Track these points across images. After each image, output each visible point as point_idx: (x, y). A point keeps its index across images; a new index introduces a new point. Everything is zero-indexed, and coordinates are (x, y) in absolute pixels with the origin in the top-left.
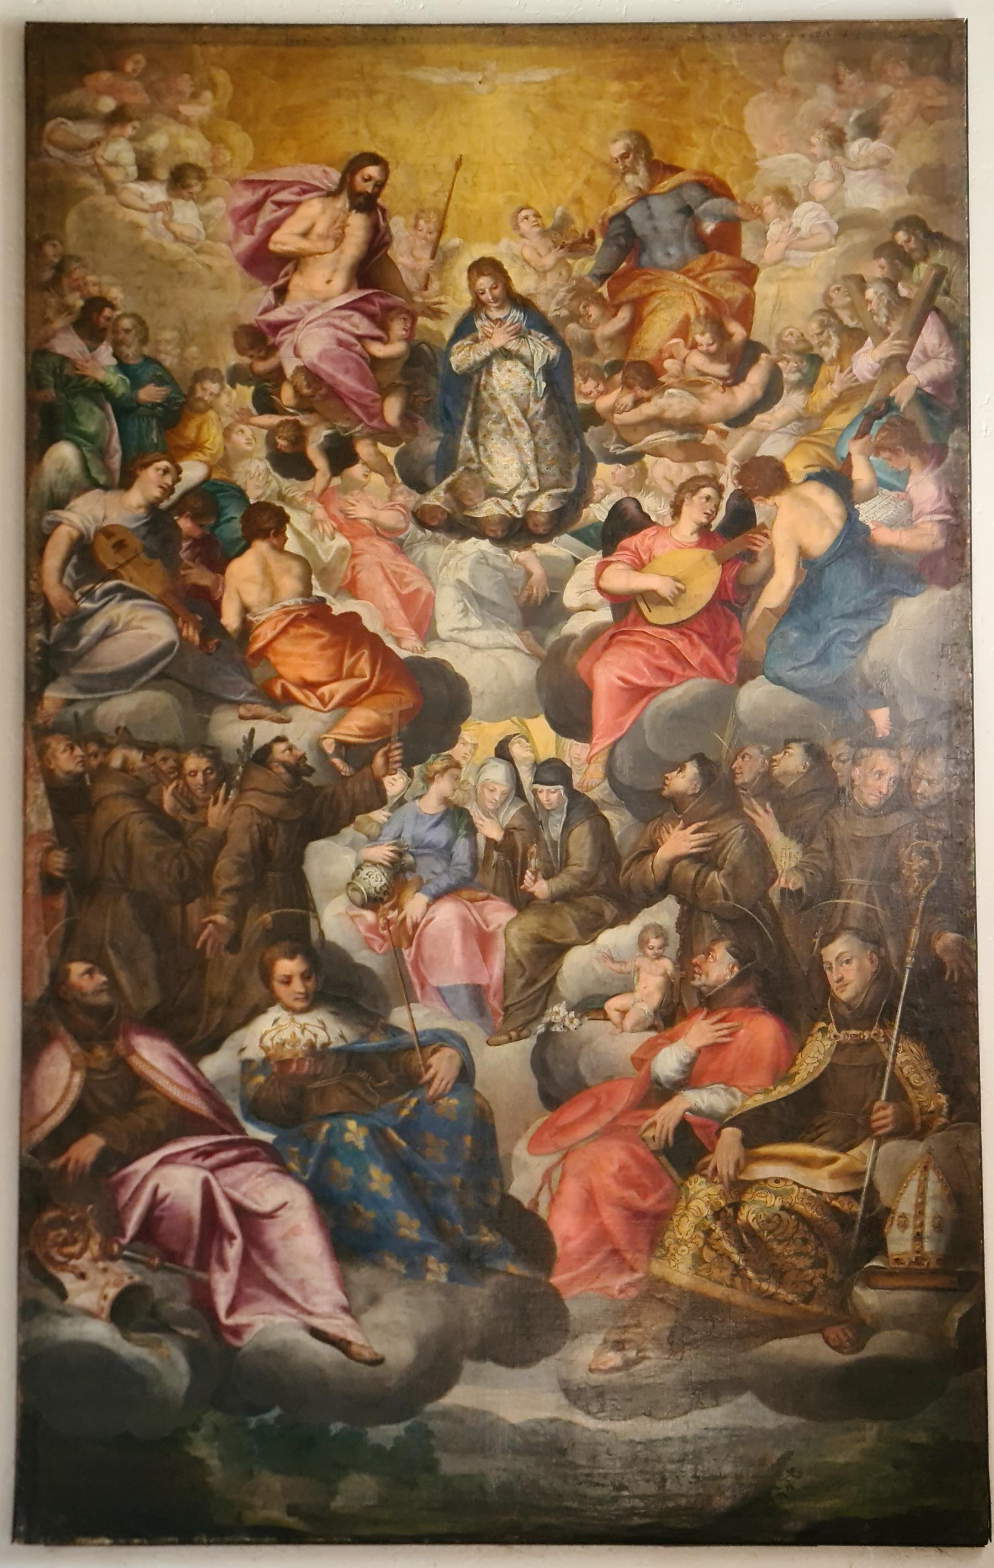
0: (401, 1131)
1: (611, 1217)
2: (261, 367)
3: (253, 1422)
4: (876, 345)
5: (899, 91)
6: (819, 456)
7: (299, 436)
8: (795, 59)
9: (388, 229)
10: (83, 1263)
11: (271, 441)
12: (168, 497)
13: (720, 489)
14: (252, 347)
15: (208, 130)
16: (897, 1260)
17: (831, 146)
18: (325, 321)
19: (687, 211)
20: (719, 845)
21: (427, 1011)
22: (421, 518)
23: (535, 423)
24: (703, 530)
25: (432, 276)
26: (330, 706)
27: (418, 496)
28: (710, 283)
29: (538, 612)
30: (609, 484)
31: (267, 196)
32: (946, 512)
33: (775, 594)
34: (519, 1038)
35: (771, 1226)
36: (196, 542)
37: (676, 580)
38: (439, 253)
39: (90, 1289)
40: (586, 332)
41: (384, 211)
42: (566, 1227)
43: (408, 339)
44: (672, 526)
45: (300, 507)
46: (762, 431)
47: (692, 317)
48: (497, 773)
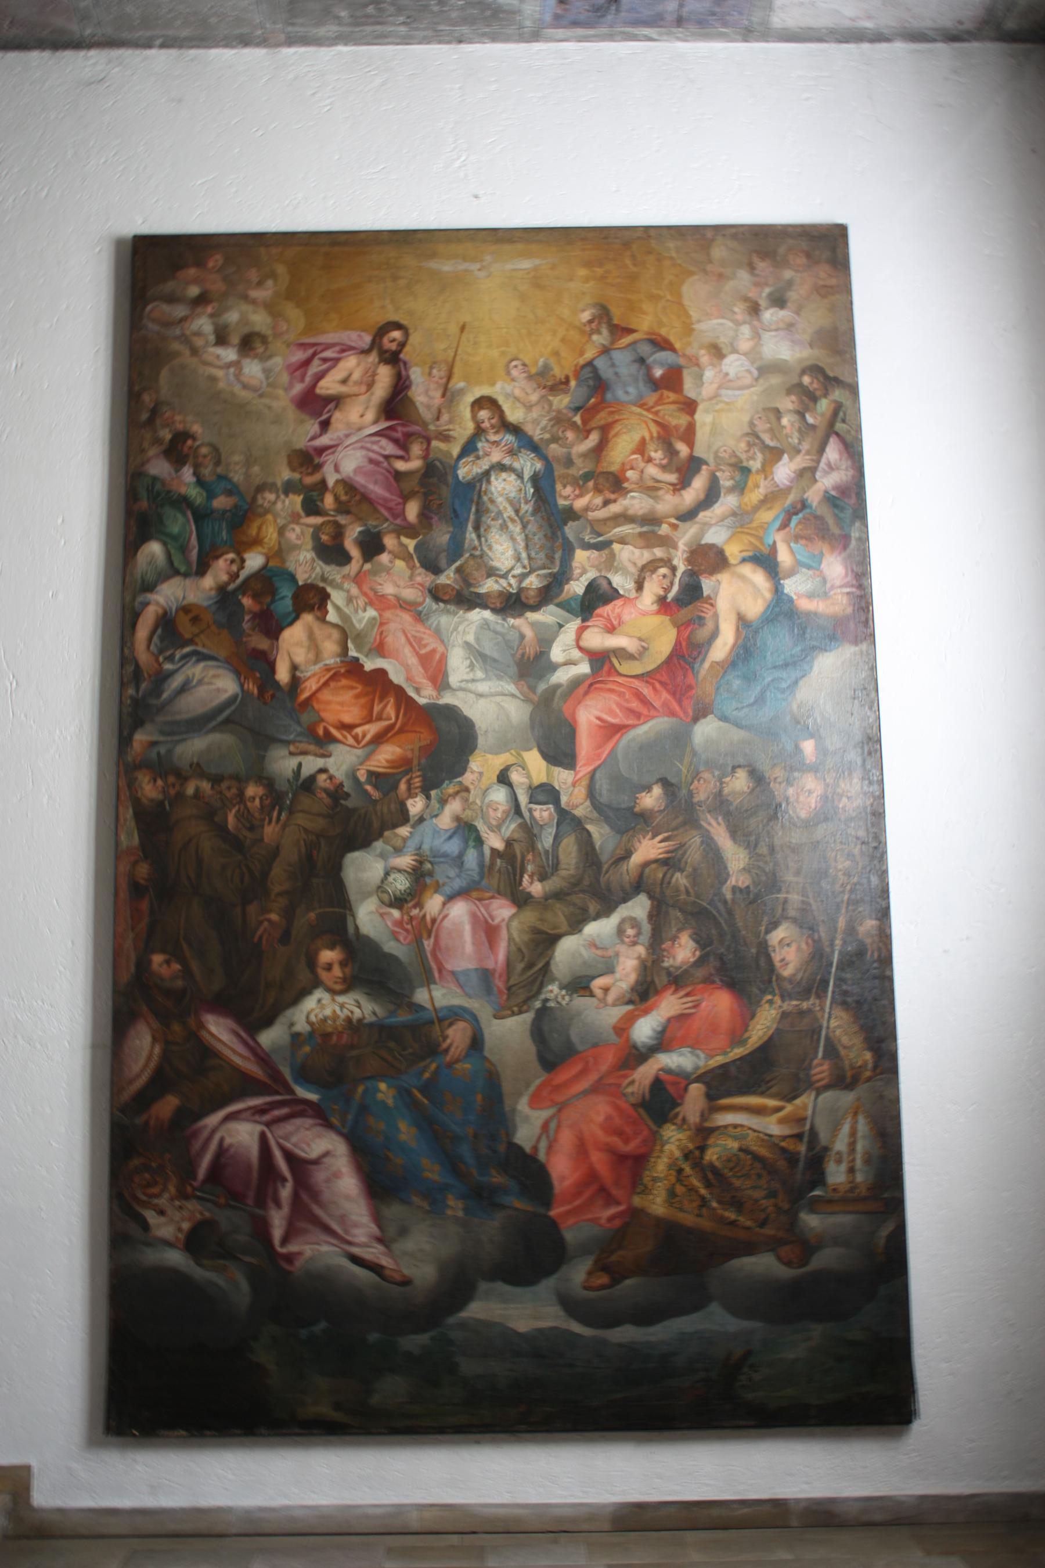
0: (422, 1091)
1: (598, 1159)
2: (309, 480)
3: (303, 1333)
4: (791, 459)
5: (799, 275)
6: (751, 543)
7: (339, 533)
8: (718, 252)
9: (408, 377)
10: (162, 1201)
11: (316, 537)
12: (234, 581)
13: (674, 569)
14: (301, 465)
15: (270, 307)
16: (834, 1190)
17: (750, 314)
18: (359, 445)
19: (641, 361)
20: (680, 852)
21: (444, 991)
22: (436, 594)
23: (525, 520)
24: (662, 601)
25: (443, 410)
26: (363, 743)
27: (433, 577)
28: (661, 414)
29: (531, 666)
30: (586, 567)
31: (314, 354)
32: (852, 586)
33: (721, 649)
34: (520, 1012)
35: (731, 1165)
36: (256, 616)
37: (640, 639)
38: (448, 394)
39: (168, 1224)
40: (565, 450)
41: (405, 363)
42: (562, 1169)
43: (425, 457)
44: (637, 598)
45: (339, 587)
46: (705, 524)
47: (647, 438)
48: (499, 795)
